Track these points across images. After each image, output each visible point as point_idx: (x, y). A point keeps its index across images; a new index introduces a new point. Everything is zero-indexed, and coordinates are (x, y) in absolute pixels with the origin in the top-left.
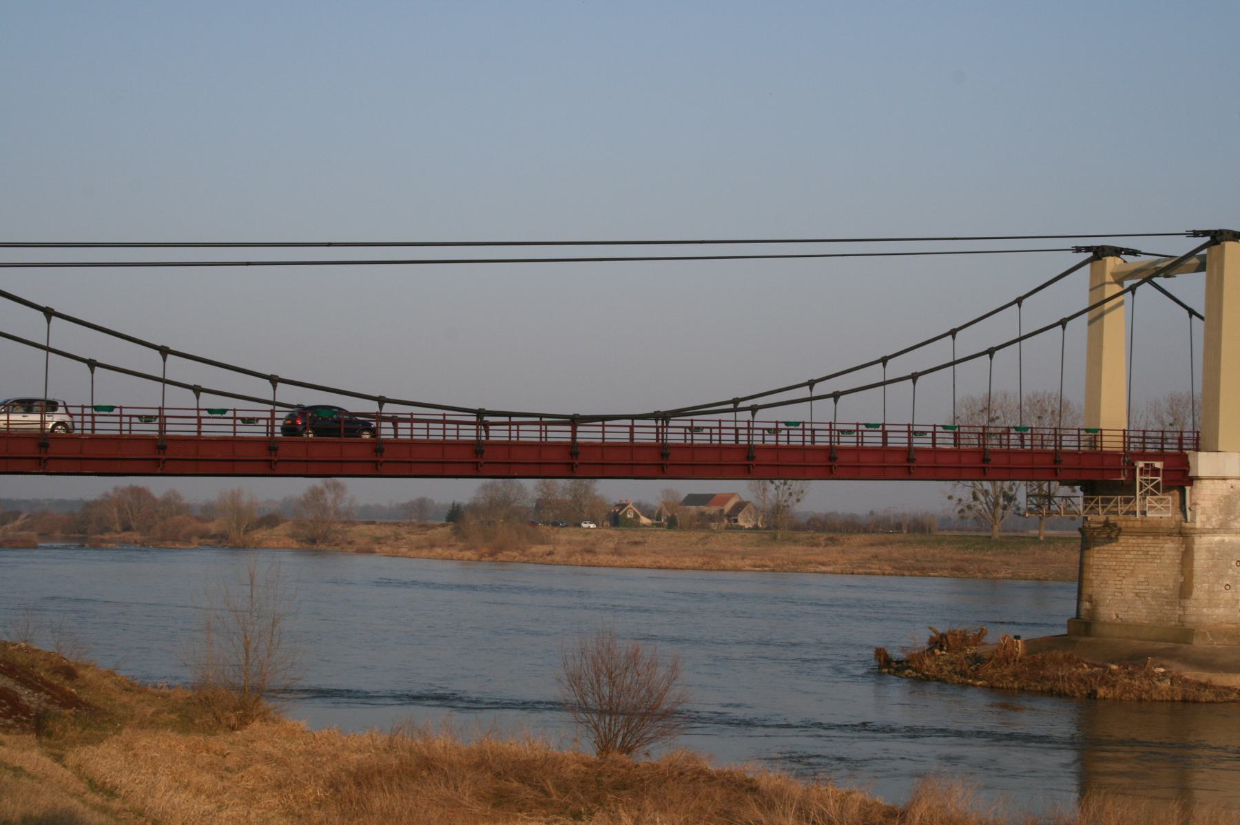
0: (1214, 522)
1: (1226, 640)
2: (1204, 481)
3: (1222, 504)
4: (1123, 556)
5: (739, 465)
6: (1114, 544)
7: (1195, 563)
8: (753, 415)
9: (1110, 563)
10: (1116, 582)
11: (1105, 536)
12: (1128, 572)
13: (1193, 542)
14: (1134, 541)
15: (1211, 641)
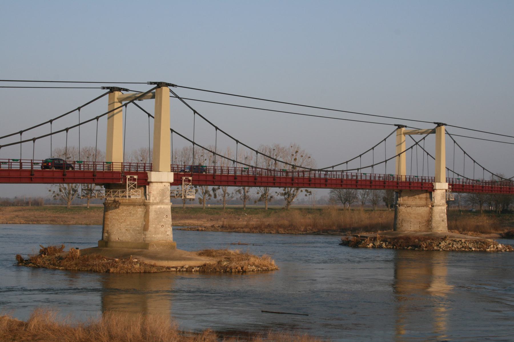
0: (158, 200)
1: (161, 247)
3: (161, 193)
6: (117, 209)
7: (150, 217)
9: (116, 217)
10: (118, 225)
12: (123, 221)
14: (126, 208)
15: (156, 248)
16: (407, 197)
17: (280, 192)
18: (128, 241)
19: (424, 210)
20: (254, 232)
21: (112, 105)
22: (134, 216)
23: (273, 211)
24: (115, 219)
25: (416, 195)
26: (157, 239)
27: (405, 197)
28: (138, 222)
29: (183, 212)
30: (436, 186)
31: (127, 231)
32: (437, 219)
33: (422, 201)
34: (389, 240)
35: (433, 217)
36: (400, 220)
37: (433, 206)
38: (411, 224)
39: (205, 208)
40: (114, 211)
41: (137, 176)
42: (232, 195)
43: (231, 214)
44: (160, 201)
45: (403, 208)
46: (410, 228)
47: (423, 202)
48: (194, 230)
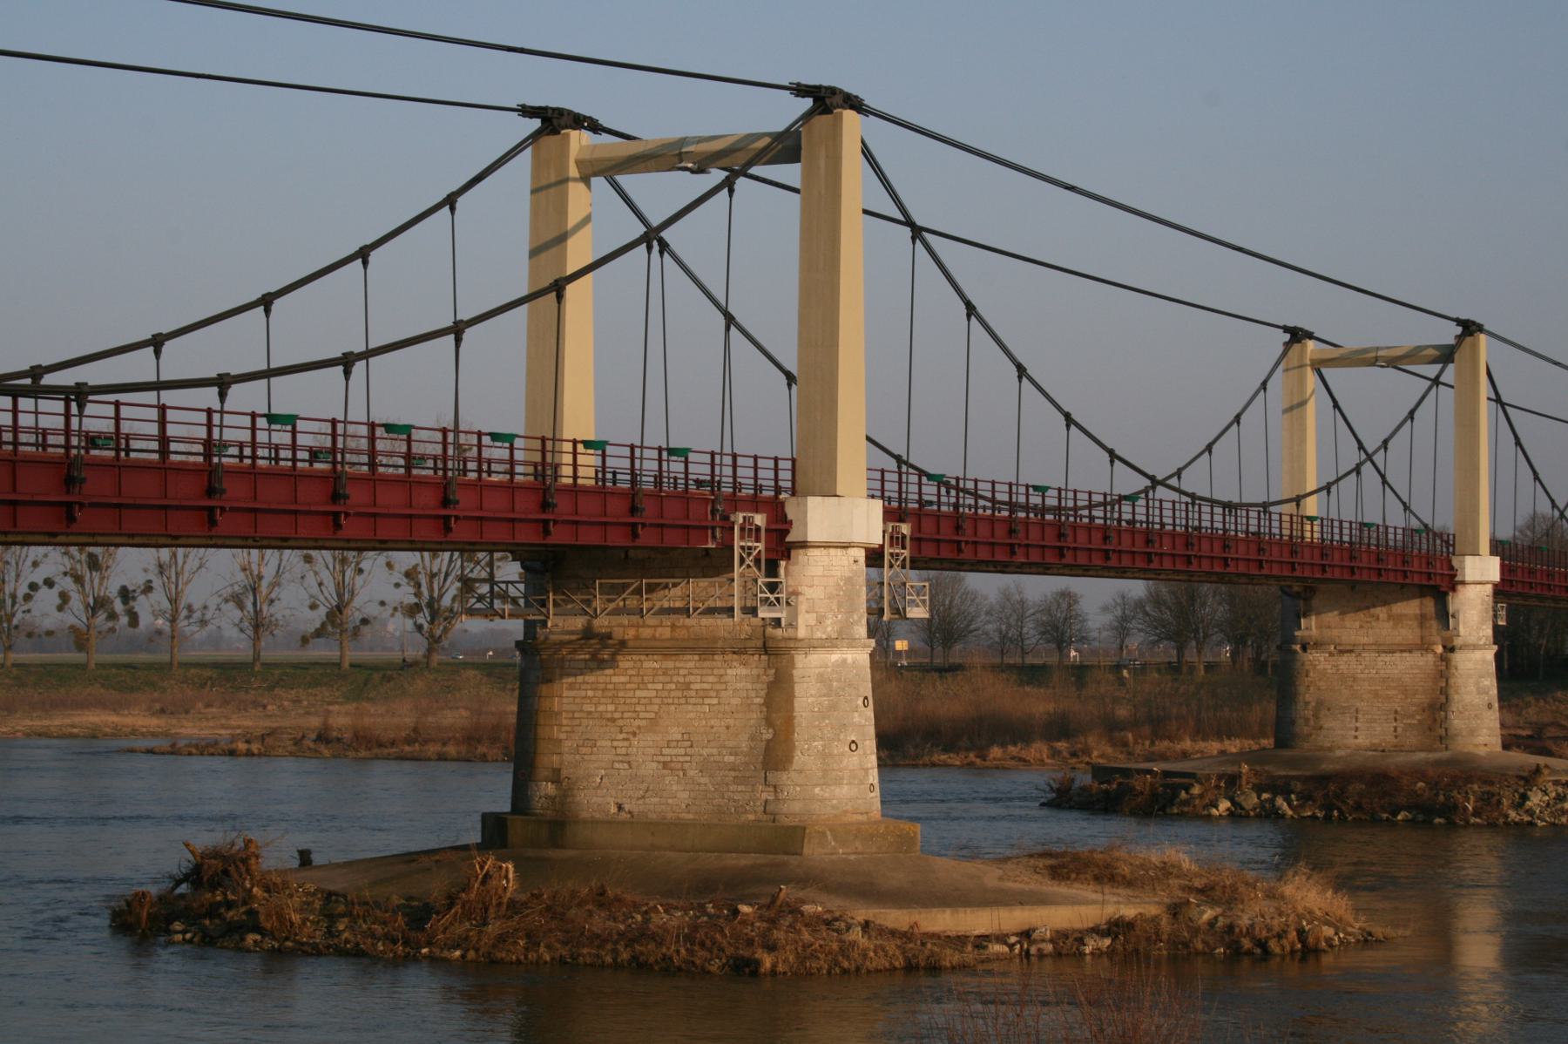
0: (830, 628)
1: (858, 845)
2: (811, 550)
3: (841, 593)
4: (631, 694)
5: (120, 515)
6: (609, 672)
7: (796, 705)
8: (222, 396)
9: (601, 708)
10: (615, 744)
11: (587, 657)
12: (643, 723)
13: (792, 663)
14: (656, 665)
15: (834, 848)
16: (1336, 613)
17: (402, 603)
18: (679, 818)
19: (1412, 667)
20: (490, 759)
21: (552, 190)
22: (707, 701)
23: (376, 677)
24: (596, 715)
25: (1374, 606)
26: (834, 807)
27: (1330, 614)
28: (728, 727)
29: (6, 681)
30: (1463, 568)
31: (666, 772)
32: (1467, 698)
33: (1403, 631)
34: (1299, 786)
35: (1451, 691)
36: (1307, 703)
37: (1452, 650)
38: (1357, 721)
39: (96, 664)
40: (590, 678)
41: (765, 515)
42: (203, 615)
43: (208, 688)
44: (840, 632)
45: (1322, 659)
46: (1356, 737)
47: (1409, 633)
48: (212, 754)
